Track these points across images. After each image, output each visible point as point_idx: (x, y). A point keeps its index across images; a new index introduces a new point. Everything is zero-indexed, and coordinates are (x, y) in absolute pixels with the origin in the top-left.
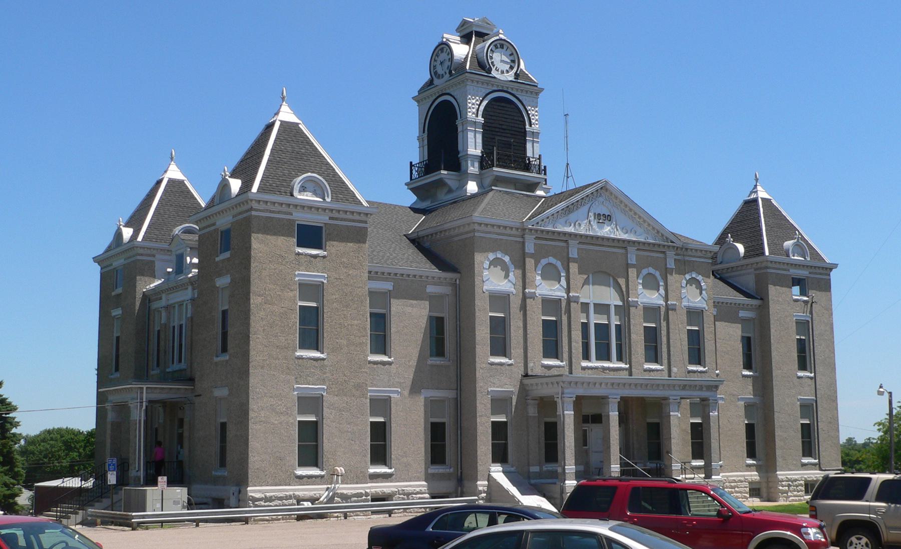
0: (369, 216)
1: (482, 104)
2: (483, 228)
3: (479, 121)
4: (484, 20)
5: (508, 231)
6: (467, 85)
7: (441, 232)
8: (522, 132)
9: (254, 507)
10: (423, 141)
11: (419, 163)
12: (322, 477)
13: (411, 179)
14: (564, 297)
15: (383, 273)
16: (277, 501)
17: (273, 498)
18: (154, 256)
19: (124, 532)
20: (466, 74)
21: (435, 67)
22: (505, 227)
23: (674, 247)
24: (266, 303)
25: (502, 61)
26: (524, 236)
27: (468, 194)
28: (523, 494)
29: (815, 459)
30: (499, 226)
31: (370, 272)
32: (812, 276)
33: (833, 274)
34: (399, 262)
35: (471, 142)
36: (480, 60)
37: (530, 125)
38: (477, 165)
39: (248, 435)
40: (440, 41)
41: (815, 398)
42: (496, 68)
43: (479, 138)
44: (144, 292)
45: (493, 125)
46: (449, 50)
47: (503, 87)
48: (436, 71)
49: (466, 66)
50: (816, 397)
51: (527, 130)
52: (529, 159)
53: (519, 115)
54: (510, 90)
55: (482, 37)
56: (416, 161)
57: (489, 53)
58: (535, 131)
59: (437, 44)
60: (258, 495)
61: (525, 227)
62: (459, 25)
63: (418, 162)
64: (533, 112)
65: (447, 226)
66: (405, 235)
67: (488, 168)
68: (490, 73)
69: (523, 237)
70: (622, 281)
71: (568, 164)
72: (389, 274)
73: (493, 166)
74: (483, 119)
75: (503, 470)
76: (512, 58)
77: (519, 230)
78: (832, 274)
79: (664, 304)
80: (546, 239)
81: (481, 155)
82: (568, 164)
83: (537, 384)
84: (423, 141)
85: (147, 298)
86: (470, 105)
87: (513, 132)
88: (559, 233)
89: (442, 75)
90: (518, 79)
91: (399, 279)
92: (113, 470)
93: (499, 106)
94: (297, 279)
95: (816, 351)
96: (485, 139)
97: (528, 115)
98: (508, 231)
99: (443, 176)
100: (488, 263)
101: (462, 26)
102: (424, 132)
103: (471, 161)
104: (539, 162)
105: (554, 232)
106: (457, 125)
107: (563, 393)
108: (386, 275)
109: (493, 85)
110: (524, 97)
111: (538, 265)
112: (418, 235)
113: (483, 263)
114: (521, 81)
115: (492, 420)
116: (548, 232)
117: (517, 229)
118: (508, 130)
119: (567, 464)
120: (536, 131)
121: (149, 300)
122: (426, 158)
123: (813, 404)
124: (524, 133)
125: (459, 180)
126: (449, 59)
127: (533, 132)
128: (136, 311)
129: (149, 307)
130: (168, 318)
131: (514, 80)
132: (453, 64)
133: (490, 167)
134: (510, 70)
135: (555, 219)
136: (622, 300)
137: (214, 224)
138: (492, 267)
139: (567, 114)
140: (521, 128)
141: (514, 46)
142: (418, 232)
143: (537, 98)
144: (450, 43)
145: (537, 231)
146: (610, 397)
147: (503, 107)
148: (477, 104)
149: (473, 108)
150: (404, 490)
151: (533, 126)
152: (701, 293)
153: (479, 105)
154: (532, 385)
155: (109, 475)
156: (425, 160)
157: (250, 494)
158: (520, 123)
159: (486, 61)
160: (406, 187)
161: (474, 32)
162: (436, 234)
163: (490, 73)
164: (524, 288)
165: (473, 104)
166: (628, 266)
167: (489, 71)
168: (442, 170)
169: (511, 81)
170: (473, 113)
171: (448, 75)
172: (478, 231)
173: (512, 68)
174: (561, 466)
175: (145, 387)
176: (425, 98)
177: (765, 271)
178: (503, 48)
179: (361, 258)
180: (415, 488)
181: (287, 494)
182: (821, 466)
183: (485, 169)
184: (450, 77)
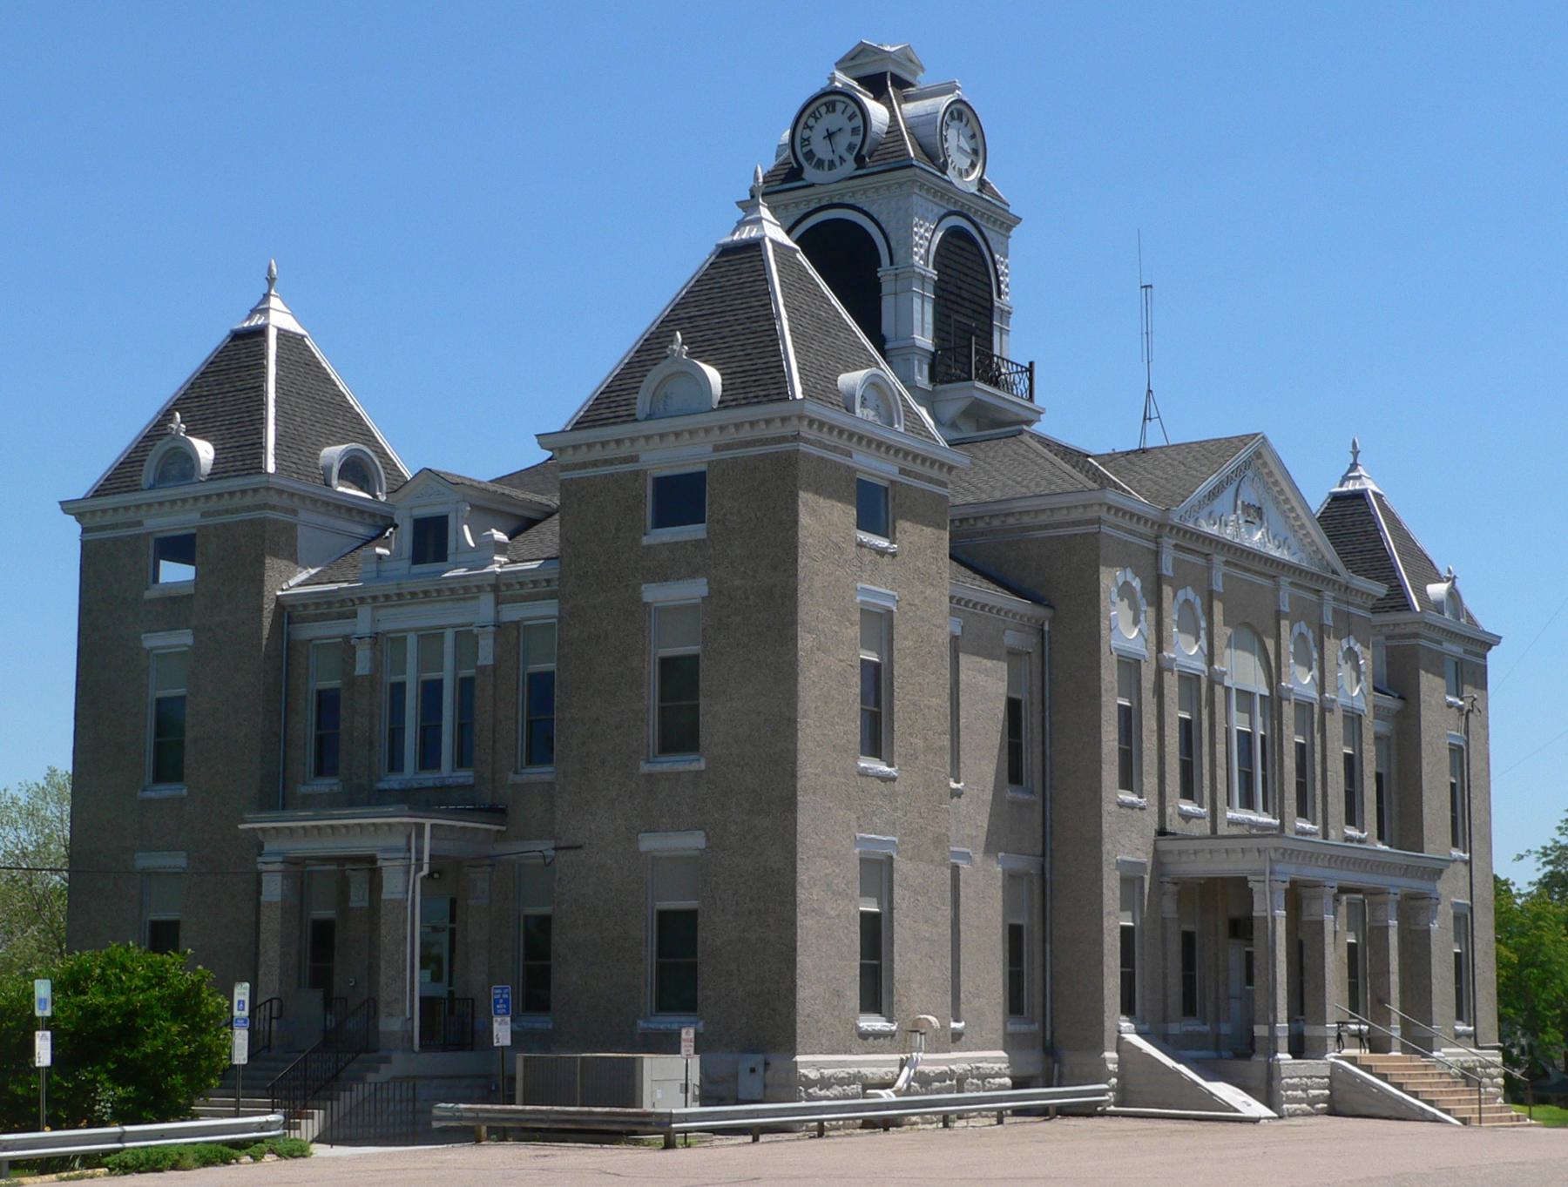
9: (807, 1101)
12: (891, 1035)
14: (1203, 672)
16: (836, 1087)
17: (833, 1080)
18: (294, 512)
19: (546, 1159)
21: (806, 141)
23: (1335, 582)
24: (818, 649)
25: (960, 148)
26: (1159, 540)
28: (1207, 1080)
29: (1469, 1025)
31: (951, 598)
32: (1468, 657)
33: (1493, 656)
37: (999, 294)
39: (795, 942)
41: (1468, 902)
43: (929, 309)
44: (278, 597)
47: (963, 205)
50: (1471, 900)
59: (815, 89)
60: (813, 1074)
62: (847, 55)
69: (1157, 539)
70: (1270, 644)
75: (1136, 1029)
78: (1490, 655)
79: (1318, 698)
81: (933, 349)
83: (1180, 853)
85: (287, 611)
87: (975, 307)
92: (504, 1014)
94: (859, 599)
95: (1472, 810)
101: (852, 59)
107: (1271, 873)
114: (987, 198)
115: (1122, 923)
119: (1279, 1020)
121: (289, 617)
123: (1466, 916)
124: (989, 309)
128: (264, 642)
129: (288, 634)
130: (376, 664)
131: (977, 193)
132: (868, 141)
136: (1270, 685)
137: (634, 459)
139: (1151, 286)
140: (986, 300)
143: (1009, 237)
146: (1326, 884)
147: (962, 249)
149: (921, 246)
150: (978, 1068)
152: (1358, 681)
154: (1171, 852)
155: (496, 1026)
157: (802, 1071)
163: (945, 173)
164: (1160, 649)
166: (1278, 615)
169: (972, 194)
174: (1268, 1024)
175: (428, 822)
177: (1412, 642)
180: (991, 1065)
181: (851, 1071)
182: (1478, 1039)
184: (857, 169)
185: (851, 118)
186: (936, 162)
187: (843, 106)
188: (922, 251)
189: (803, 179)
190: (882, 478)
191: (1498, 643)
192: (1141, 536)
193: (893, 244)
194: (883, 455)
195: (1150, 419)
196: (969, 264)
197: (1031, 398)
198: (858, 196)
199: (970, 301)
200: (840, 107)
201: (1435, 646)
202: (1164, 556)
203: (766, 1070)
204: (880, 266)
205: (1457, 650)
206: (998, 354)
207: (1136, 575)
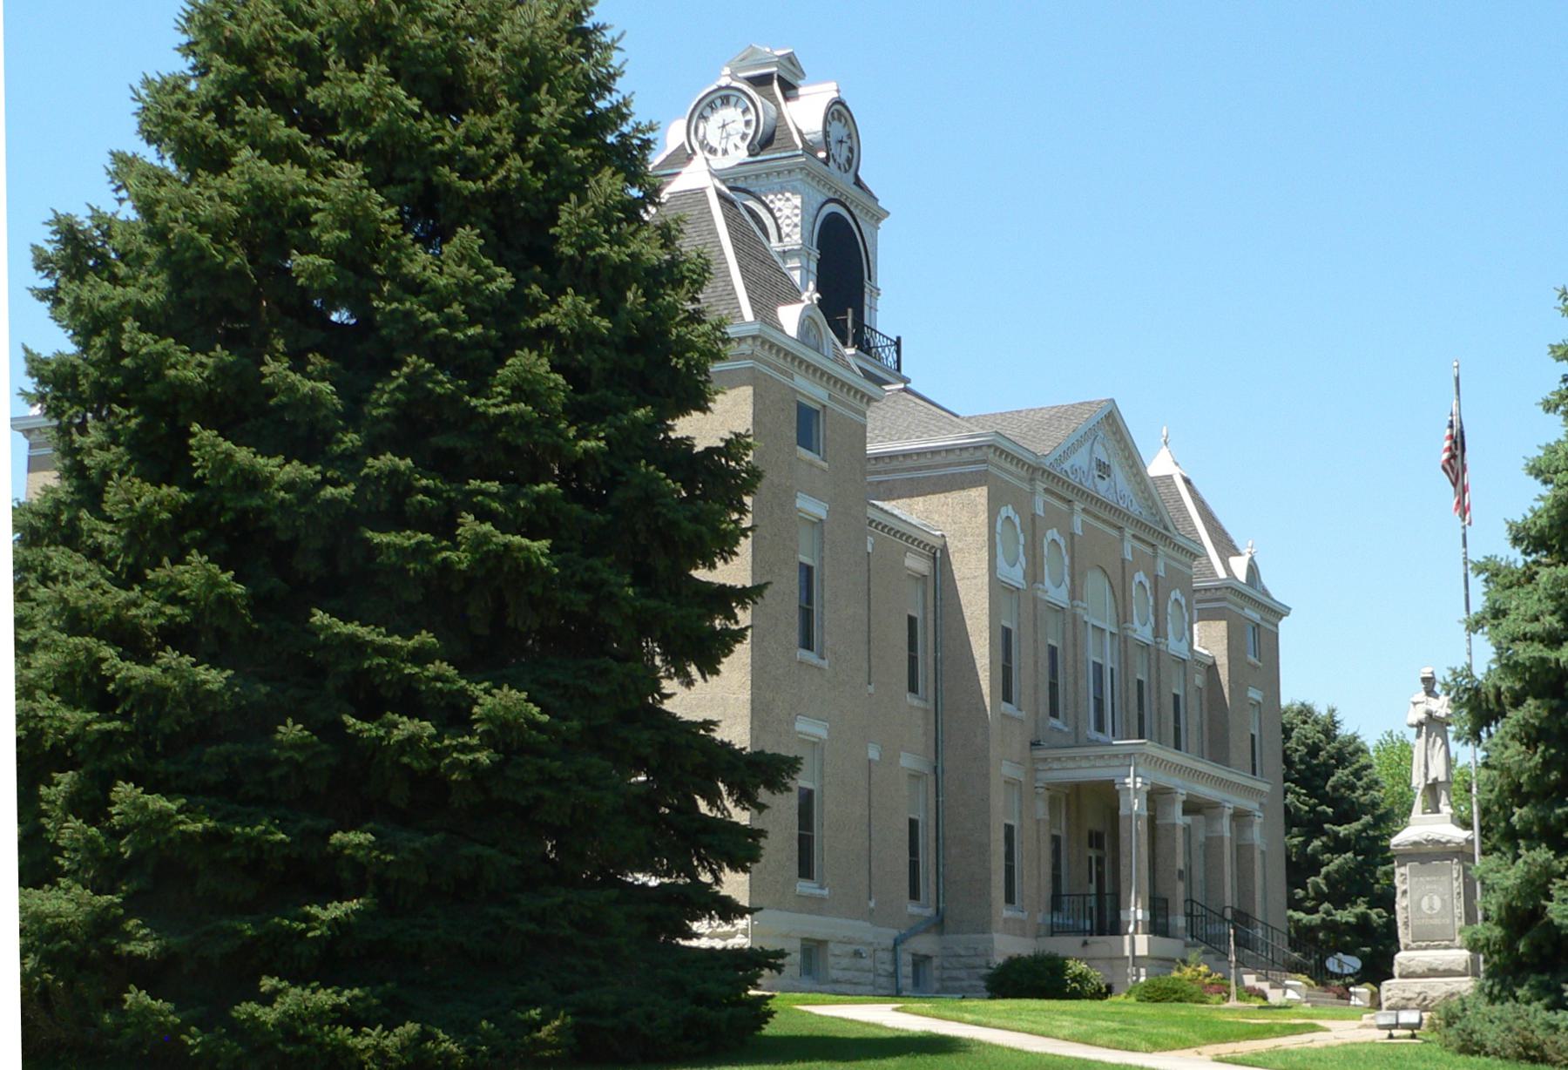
190: (816, 401)
191: (1287, 614)
194: (817, 380)
197: (899, 369)
198: (749, 181)
200: (733, 100)
201: (1240, 612)
203: (1452, 422)
205: (1255, 615)
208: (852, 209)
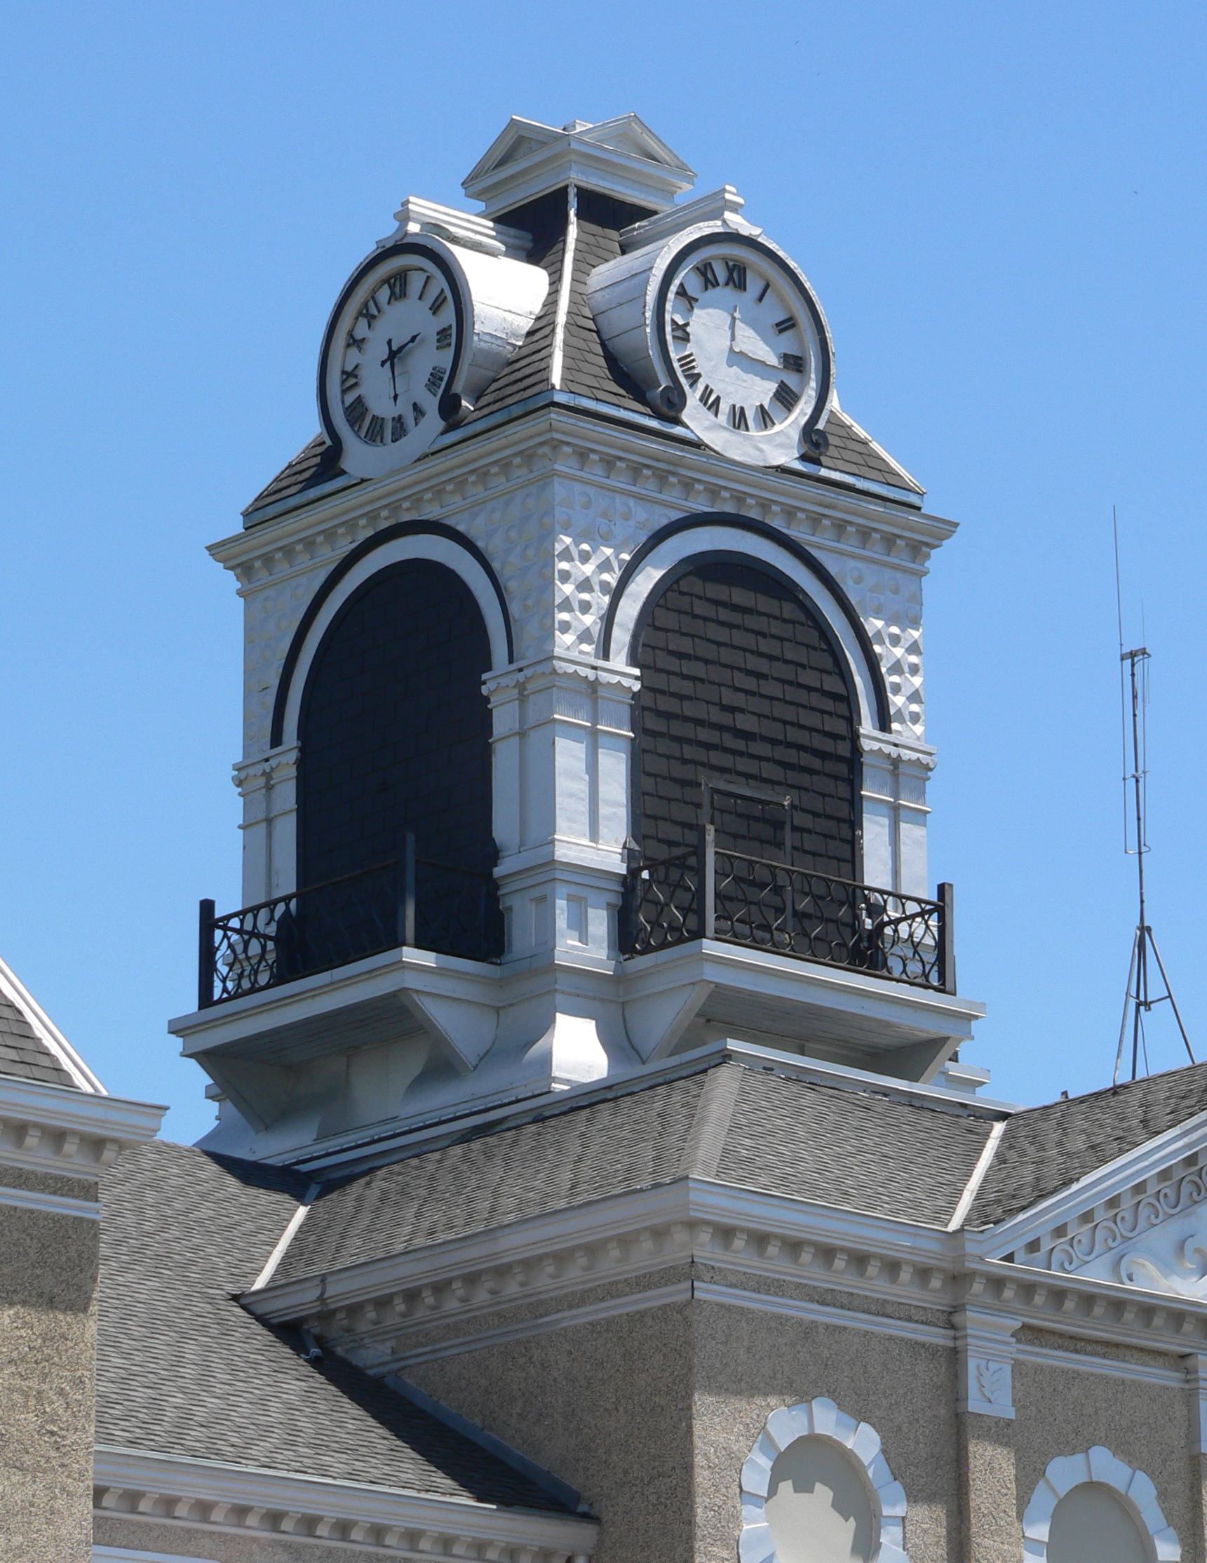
0: (109, 1154)
1: (632, 588)
2: (741, 1257)
3: (615, 679)
4: (625, 134)
5: (876, 1285)
6: (554, 473)
7: (472, 1279)
8: (841, 759)
10: (269, 788)
11: (241, 914)
13: (206, 999)
15: (168, 1504)
20: (554, 415)
21: (350, 377)
22: (860, 1260)
25: (737, 358)
26: (957, 1319)
27: (557, 1087)
30: (827, 1253)
31: (99, 1493)
34: (248, 1445)
35: (571, 795)
36: (617, 345)
37: (884, 721)
38: (599, 923)
40: (386, 230)
42: (707, 392)
45: (689, 709)
46: (440, 282)
47: (740, 498)
48: (359, 399)
49: (548, 368)
51: (866, 745)
52: (876, 911)
53: (827, 662)
54: (777, 523)
55: (617, 227)
56: (228, 903)
57: (669, 306)
58: (907, 755)
59: (367, 249)
61: (971, 1265)
63: (239, 908)
64: (899, 652)
65: (515, 1244)
66: (235, 1298)
67: (664, 945)
68: (677, 421)
69: (950, 1319)
71: (1144, 930)
72: (204, 1509)
73: (699, 934)
74: (637, 672)
76: (787, 343)
77: (936, 1283)
80: (1075, 1343)
81: (622, 869)
82: (1144, 930)
84: (269, 788)
86: (568, 589)
87: (791, 756)
88: (1148, 1310)
89: (399, 420)
90: (817, 462)
91: (255, 1540)
93: (717, 603)
96: (648, 784)
97: (872, 662)
98: (876, 1285)
99: (411, 981)
100: (766, 1463)
101: (502, 163)
102: (276, 739)
103: (570, 898)
104: (942, 929)
105: (1118, 1305)
106: (487, 700)
108: (183, 1516)
109: (688, 486)
110: (852, 563)
111: (1031, 1489)
112: (321, 1298)
113: (736, 1463)
116: (1088, 1299)
117: (923, 1273)
118: (764, 739)
120: (914, 755)
122: (287, 883)
125: (497, 1010)
126: (443, 334)
127: (896, 762)
131: (798, 466)
133: (680, 940)
134: (776, 411)
135: (1123, 1229)
138: (786, 1487)
139: (1143, 652)
140: (835, 737)
141: (803, 278)
142: (323, 1279)
144: (455, 249)
145: (1028, 1289)
148: (604, 586)
149: (585, 607)
151: (895, 726)
153: (617, 594)
156: (277, 894)
158: (828, 705)
159: (653, 352)
160: (177, 1043)
161: (572, 193)
162: (440, 1288)
163: (677, 421)
165: (585, 585)
167: (670, 403)
168: (404, 944)
169: (783, 470)
170: (585, 636)
171: (433, 421)
172: (716, 1274)
173: (786, 398)
176: (288, 551)
178: (742, 286)
179: (59, 1405)
183: (648, 949)
185: (436, 308)
186: (649, 395)
187: (423, 276)
188: (589, 620)
189: (343, 472)
192: (906, 1314)
193: (514, 609)
195: (1147, 1005)
196: (765, 646)
199: (774, 742)
200: (416, 282)
202: (972, 1365)
204: (489, 669)
206: (884, 882)
207: (860, 1412)
208: (797, 533)
